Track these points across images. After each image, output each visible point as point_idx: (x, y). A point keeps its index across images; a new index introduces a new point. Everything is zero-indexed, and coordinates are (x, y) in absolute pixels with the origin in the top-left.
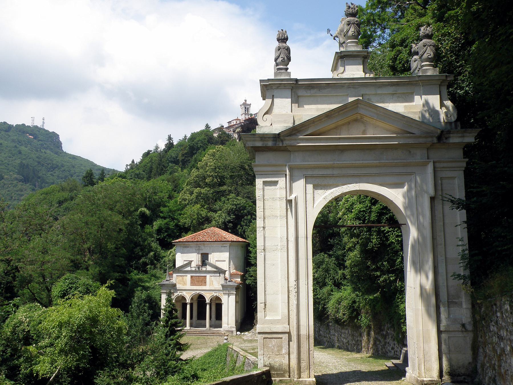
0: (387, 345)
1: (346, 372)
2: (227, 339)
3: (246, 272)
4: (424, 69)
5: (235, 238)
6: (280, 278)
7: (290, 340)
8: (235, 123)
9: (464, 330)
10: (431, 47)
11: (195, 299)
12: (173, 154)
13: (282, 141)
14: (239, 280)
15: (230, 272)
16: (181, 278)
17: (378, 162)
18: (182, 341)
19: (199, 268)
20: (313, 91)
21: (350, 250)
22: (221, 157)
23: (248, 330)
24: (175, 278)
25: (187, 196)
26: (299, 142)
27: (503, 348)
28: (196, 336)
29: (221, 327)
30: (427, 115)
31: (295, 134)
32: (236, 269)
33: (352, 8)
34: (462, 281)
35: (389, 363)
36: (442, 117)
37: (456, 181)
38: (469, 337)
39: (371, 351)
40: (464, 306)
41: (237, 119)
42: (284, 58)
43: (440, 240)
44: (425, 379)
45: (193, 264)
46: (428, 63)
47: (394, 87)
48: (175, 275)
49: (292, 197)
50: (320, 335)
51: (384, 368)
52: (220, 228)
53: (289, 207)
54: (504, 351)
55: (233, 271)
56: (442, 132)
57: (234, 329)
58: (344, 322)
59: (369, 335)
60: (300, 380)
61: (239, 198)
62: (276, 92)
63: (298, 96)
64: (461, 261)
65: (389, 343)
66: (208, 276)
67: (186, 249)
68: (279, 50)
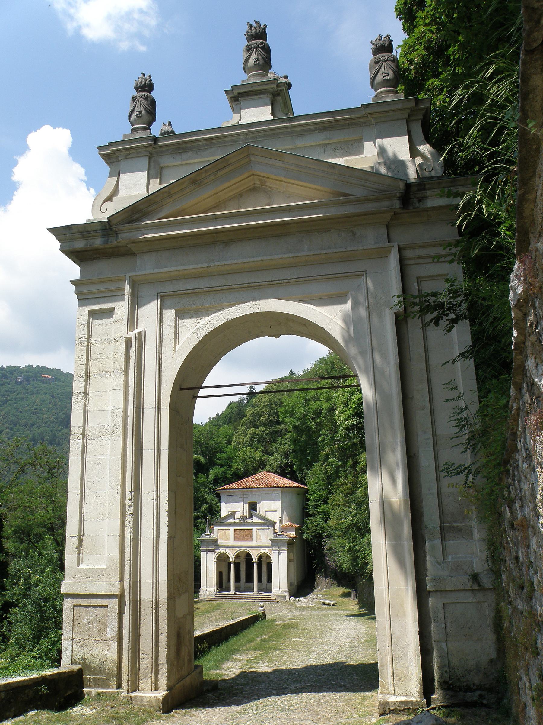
2: (262, 607)
3: (302, 524)
5: (290, 483)
9: (476, 587)
15: (281, 523)
16: (223, 532)
17: (291, 255)
19: (243, 519)
23: (305, 595)
26: (144, 232)
28: (241, 602)
31: (139, 220)
32: (290, 520)
38: (488, 603)
40: (477, 535)
43: (420, 398)
45: (238, 515)
46: (385, 89)
55: (286, 523)
57: (287, 594)
60: (133, 695)
66: (254, 529)
67: (231, 498)
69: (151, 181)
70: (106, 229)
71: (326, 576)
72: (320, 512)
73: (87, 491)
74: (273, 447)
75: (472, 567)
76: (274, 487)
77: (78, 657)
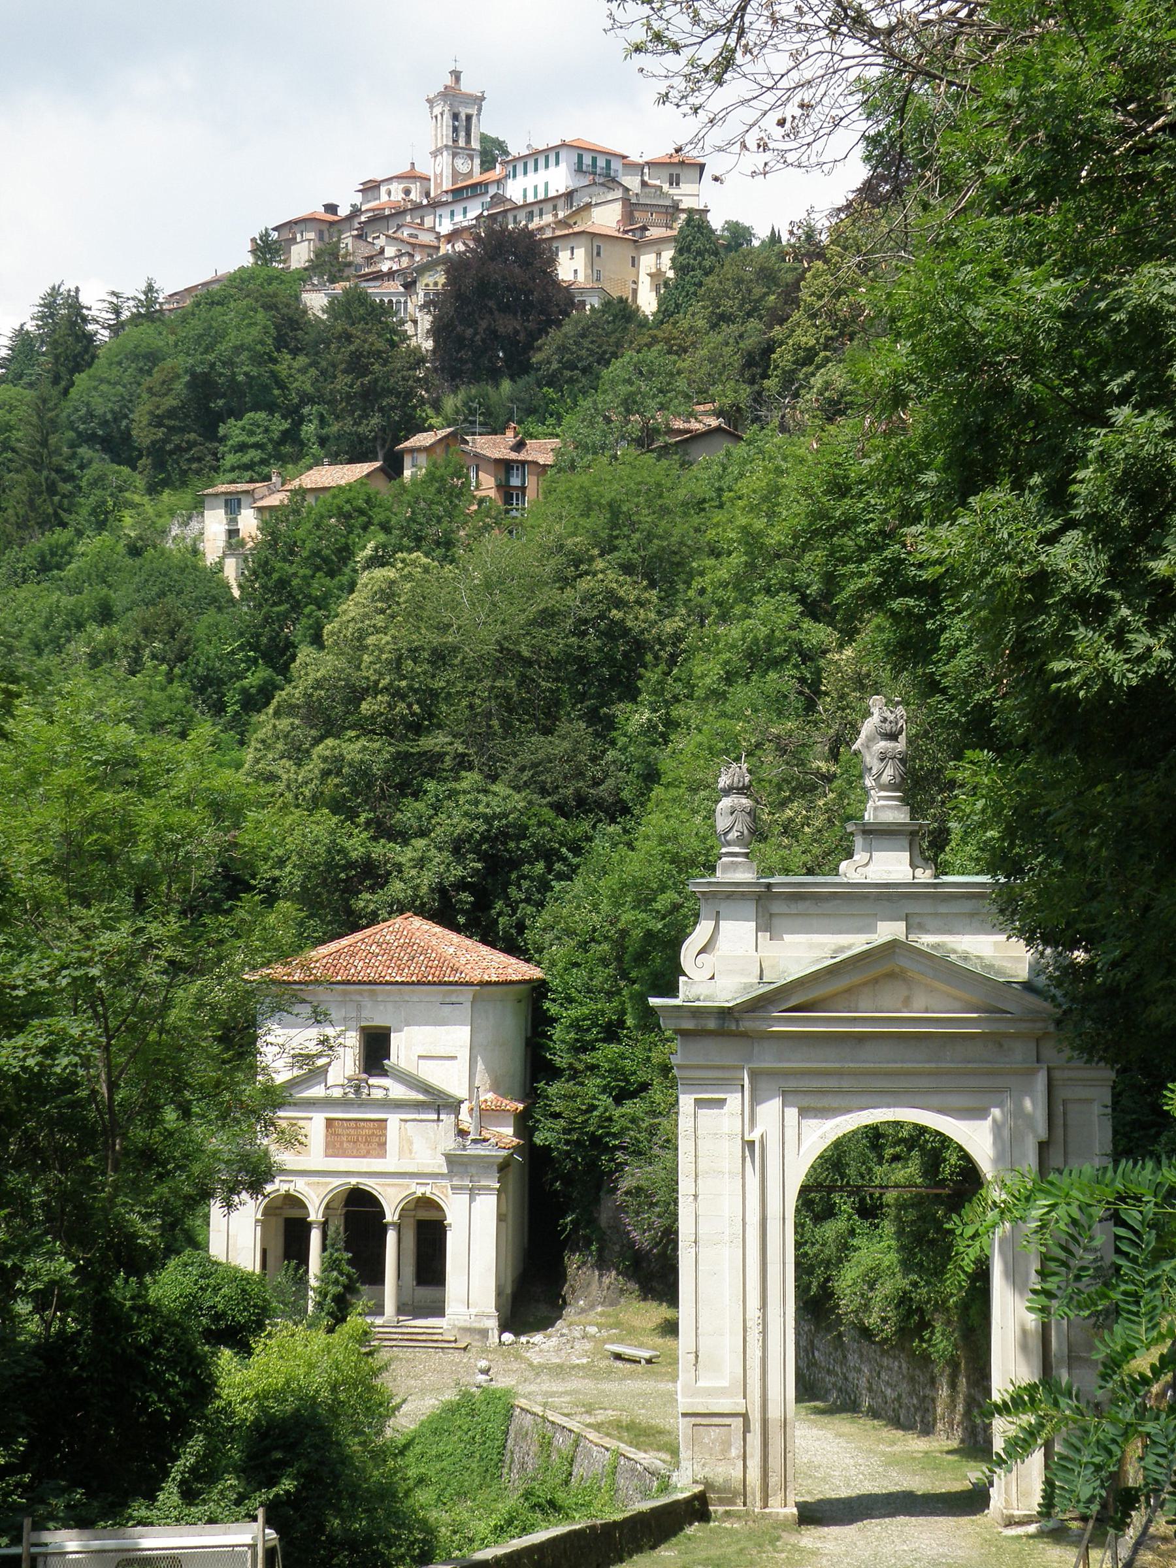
2: (485, 1372)
3: (531, 1095)
7: (746, 1429)
14: (510, 1131)
19: (358, 1089)
20: (802, 906)
23: (544, 1324)
32: (496, 1088)
39: (959, 1433)
41: (411, 176)
44: (1016, 1513)
49: (755, 1136)
50: (812, 1364)
57: (492, 1324)
59: (953, 1386)
62: (723, 907)
63: (771, 915)
66: (394, 1120)
71: (602, 1265)
72: (597, 1067)
74: (409, 813)
76: (450, 983)
77: (699, 1477)
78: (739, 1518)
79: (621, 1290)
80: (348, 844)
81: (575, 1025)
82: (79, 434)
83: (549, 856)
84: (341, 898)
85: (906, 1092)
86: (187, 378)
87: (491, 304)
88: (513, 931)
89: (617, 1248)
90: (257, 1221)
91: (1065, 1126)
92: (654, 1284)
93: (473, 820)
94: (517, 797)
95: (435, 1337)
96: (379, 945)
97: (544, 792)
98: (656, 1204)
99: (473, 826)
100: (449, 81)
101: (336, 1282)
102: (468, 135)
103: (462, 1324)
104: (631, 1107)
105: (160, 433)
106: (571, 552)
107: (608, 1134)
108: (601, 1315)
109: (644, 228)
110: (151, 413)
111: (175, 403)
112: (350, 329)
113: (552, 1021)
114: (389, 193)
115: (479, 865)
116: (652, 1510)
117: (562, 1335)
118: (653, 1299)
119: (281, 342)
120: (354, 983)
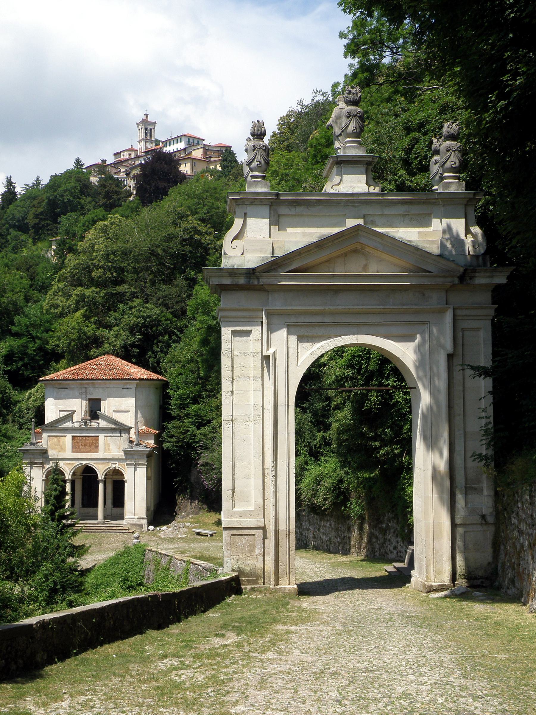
0: (387, 543)
1: (332, 579)
2: (137, 538)
3: (162, 429)
4: (446, 183)
6: (253, 458)
7: (265, 537)
8: (127, 156)
9: (483, 522)
10: (457, 152)
11: (79, 473)
12: (16, 212)
13: (258, 278)
14: (152, 442)
16: (55, 439)
18: (77, 541)
19: (86, 423)
20: (299, 210)
21: (337, 407)
22: (117, 237)
23: (167, 522)
24: (46, 440)
25: (60, 301)
26: (281, 280)
27: (522, 544)
29: (122, 518)
30: (449, 245)
31: (275, 270)
32: (146, 424)
33: (353, 94)
34: (484, 462)
35: (390, 568)
36: (469, 247)
37: (482, 333)
38: (490, 531)
39: (364, 552)
40: (485, 493)
41: (131, 150)
42: (260, 162)
43: (458, 409)
44: (434, 584)
45: (76, 418)
46: (451, 174)
47: (406, 206)
48: (45, 435)
49: (270, 352)
51: (384, 573)
52: (117, 355)
53: (265, 365)
54: (523, 547)
56: (465, 270)
57: (145, 522)
58: (326, 510)
59: (361, 529)
60: (278, 587)
61: (149, 306)
62: (249, 209)
63: (279, 216)
64: (484, 438)
65: (389, 540)
66: (101, 436)
68: (254, 150)
69: (272, 227)
70: (249, 273)
71: (192, 498)
72: (189, 414)
73: (235, 460)
75: (482, 511)
76: (126, 379)
78: (261, 592)
79: (200, 508)
80: (86, 329)
81: (181, 398)
82: (10, 225)
83: (171, 334)
84: (84, 349)
85: (365, 324)
86: (47, 201)
87: (156, 177)
88: (155, 364)
89: (198, 491)
90: (43, 480)
91: (463, 345)
92: (214, 505)
93: (138, 318)
94: (156, 309)
95: (120, 528)
96: (97, 365)
97: (168, 308)
98: (214, 469)
99: (138, 320)
100: (144, 117)
101: (56, 490)
102: (151, 135)
103: (132, 522)
104: (203, 430)
105: (37, 221)
106: (179, 213)
107: (194, 442)
108: (192, 518)
109: (211, 157)
110: (34, 214)
111: (42, 210)
112: (105, 183)
113: (170, 398)
114: (124, 156)
115: (141, 337)
116: (203, 586)
117: (175, 526)
118: (213, 512)
119: (82, 192)
120: (85, 380)
